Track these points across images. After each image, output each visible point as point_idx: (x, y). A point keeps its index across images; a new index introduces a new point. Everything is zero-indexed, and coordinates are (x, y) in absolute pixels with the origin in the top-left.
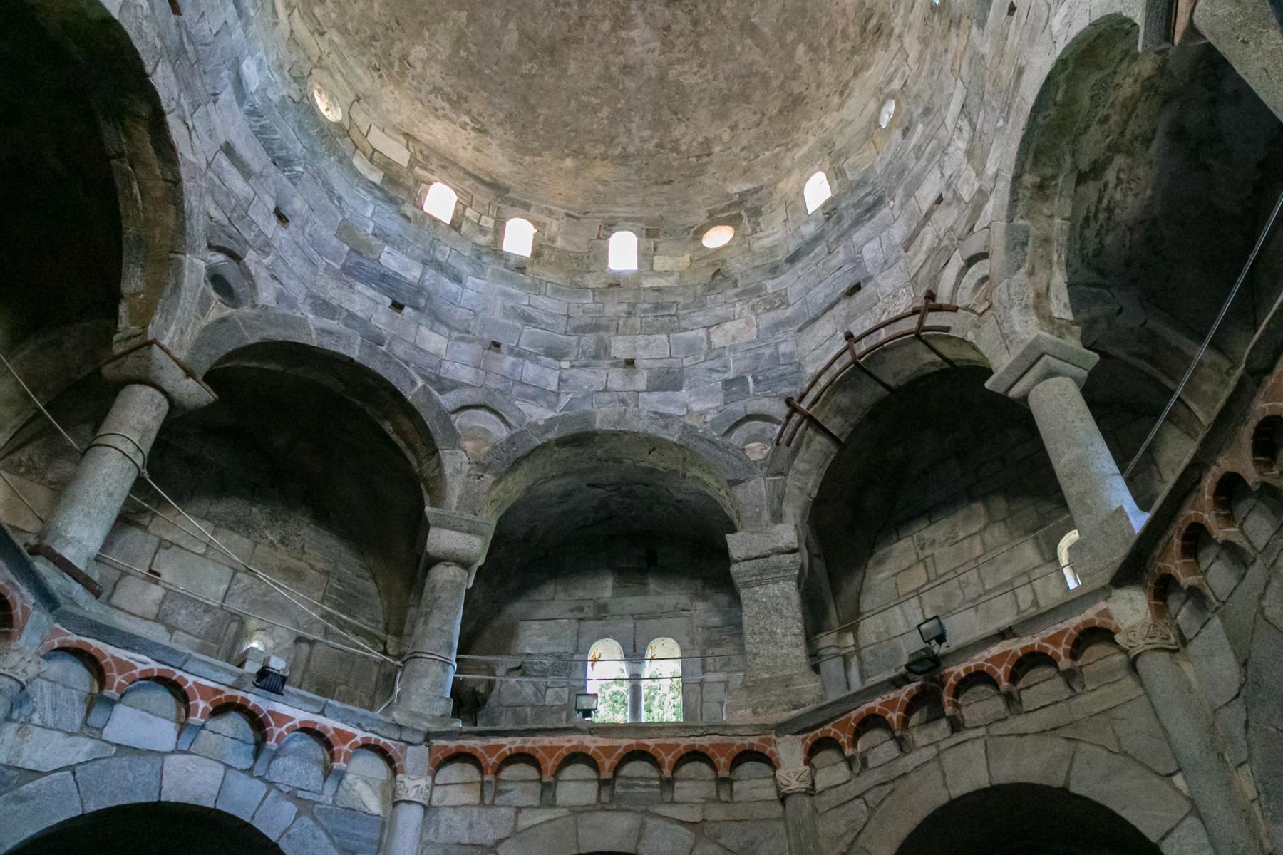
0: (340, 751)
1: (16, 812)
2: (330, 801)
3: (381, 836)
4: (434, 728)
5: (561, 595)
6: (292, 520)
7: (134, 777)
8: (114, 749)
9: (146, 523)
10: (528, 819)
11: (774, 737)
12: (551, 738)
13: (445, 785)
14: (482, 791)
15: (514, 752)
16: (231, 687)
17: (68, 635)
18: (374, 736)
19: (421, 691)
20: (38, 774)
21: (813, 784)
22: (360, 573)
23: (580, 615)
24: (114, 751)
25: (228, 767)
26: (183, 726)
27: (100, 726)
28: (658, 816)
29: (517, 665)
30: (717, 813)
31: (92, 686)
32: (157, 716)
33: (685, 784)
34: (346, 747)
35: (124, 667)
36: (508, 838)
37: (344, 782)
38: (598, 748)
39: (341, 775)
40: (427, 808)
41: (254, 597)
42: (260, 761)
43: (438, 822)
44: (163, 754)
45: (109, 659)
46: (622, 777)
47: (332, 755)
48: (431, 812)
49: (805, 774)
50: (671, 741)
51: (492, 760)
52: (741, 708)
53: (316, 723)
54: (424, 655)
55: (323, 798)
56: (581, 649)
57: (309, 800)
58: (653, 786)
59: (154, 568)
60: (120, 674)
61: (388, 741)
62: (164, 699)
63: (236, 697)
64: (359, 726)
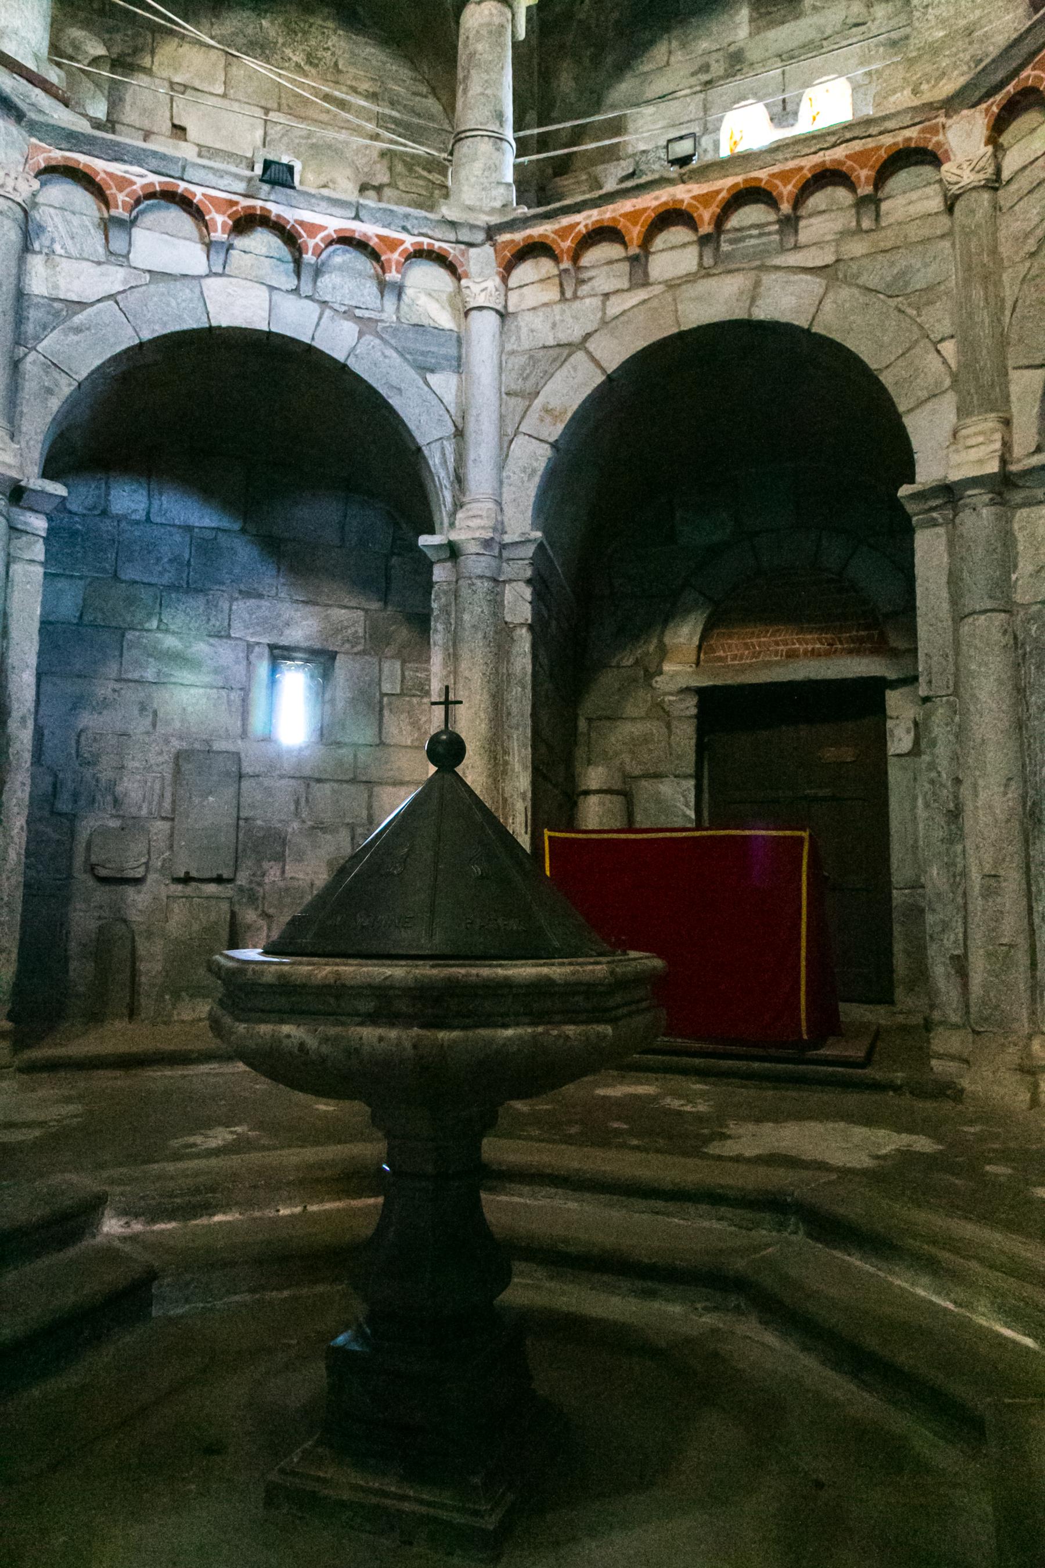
0: (389, 261)
1: (78, 343)
2: (394, 318)
3: (459, 352)
4: (495, 220)
5: (678, 56)
6: (313, 30)
7: (178, 304)
8: (147, 276)
9: (148, 65)
10: (615, 307)
11: (942, 120)
12: (634, 200)
13: (521, 287)
14: (561, 285)
15: (590, 227)
16: (246, 196)
17: (50, 151)
18: (426, 241)
19: (473, 180)
20: (82, 305)
21: (998, 171)
22: (414, 89)
23: (705, 77)
24: (148, 278)
25: (272, 288)
26: (209, 246)
27: (125, 252)
28: (777, 268)
29: (631, 170)
30: (857, 248)
31: (99, 210)
32: (179, 238)
33: (813, 220)
34: (396, 256)
35: (123, 183)
36: (596, 331)
37: (404, 297)
38: (694, 198)
39: (399, 290)
40: (503, 315)
41: (297, 141)
42: (302, 278)
43: (518, 328)
44: (200, 277)
45: (103, 175)
46: (728, 231)
47: (382, 267)
48: (509, 321)
49: (985, 159)
50: (791, 165)
51: (567, 244)
52: (894, 91)
53: (354, 231)
54: (468, 134)
55: (384, 316)
56: (710, 126)
57: (370, 319)
58: (770, 234)
59: (177, 122)
60: (121, 191)
61: (445, 245)
62: (176, 217)
63: (254, 207)
64: (405, 229)
